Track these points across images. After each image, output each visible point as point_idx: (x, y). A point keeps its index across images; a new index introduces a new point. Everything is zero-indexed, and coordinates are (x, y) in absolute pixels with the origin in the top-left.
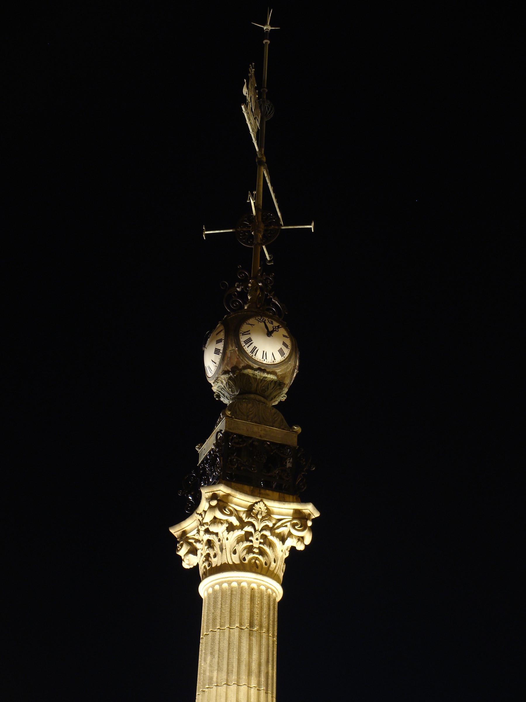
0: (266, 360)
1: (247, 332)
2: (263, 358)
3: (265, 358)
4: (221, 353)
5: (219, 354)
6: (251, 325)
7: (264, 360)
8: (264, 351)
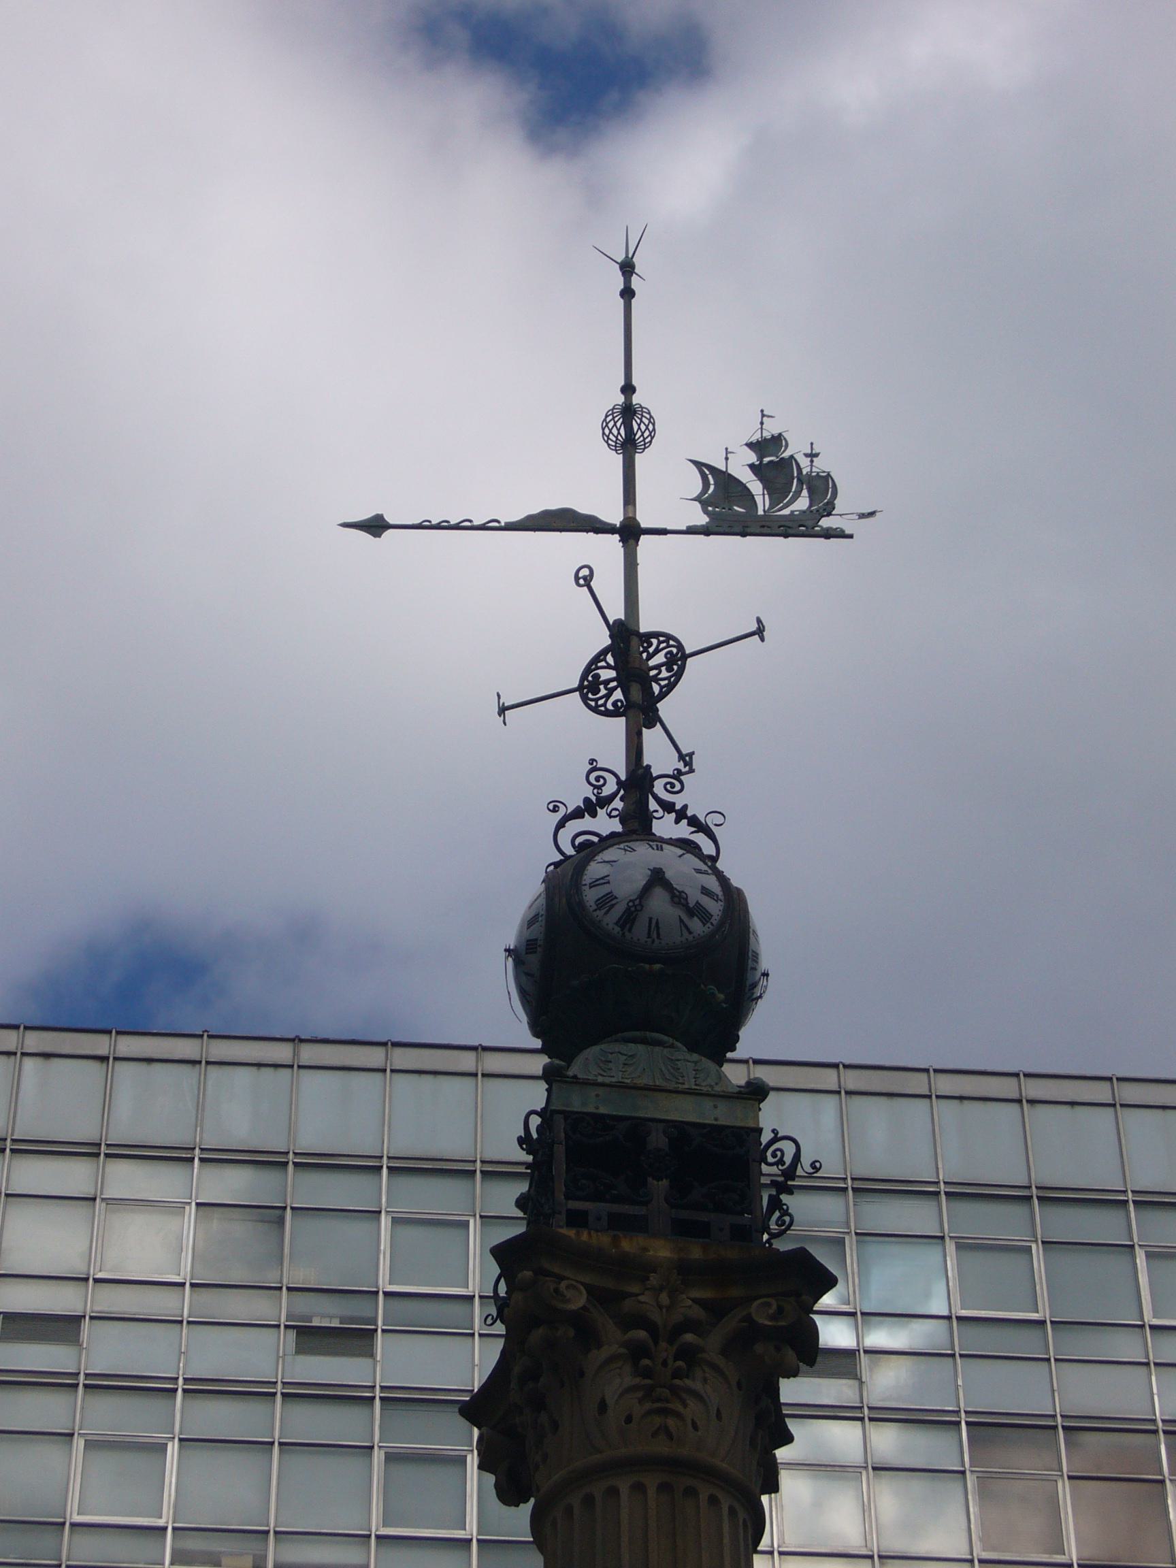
0: (657, 941)
1: (603, 878)
2: (649, 936)
3: (655, 936)
4: (540, 946)
5: (535, 952)
6: (607, 862)
7: (653, 942)
8: (650, 919)
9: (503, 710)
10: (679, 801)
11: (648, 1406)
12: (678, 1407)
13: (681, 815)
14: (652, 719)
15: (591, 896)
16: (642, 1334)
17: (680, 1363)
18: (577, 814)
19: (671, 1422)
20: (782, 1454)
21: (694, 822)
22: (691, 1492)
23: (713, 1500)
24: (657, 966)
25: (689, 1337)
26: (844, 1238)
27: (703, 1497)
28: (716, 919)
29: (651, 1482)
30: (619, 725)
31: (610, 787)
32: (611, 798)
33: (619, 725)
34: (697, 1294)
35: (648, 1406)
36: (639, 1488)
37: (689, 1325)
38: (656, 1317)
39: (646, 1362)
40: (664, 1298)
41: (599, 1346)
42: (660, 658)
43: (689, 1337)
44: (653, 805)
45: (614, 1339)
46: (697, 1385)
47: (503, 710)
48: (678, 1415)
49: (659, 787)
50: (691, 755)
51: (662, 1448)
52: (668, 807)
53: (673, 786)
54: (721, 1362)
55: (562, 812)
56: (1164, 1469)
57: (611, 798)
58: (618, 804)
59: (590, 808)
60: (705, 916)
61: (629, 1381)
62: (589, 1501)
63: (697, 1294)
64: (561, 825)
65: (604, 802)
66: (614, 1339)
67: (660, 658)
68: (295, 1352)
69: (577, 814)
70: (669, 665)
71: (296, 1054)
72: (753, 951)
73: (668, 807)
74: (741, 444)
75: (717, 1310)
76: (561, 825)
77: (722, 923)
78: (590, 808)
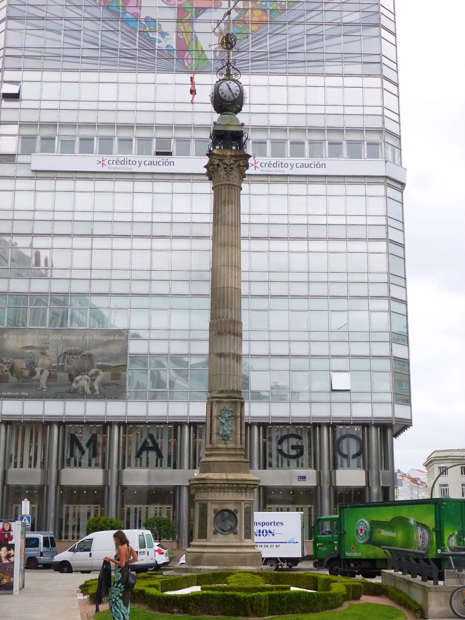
9: (210, 46)
11: (227, 176)
12: (230, 176)
15: (220, 92)
19: (229, 179)
22: (232, 188)
23: (235, 189)
24: (230, 103)
27: (233, 189)
28: (238, 95)
29: (226, 187)
35: (227, 176)
36: (225, 188)
37: (232, 164)
38: (227, 163)
39: (226, 170)
40: (229, 160)
41: (220, 167)
45: (222, 166)
46: (233, 173)
47: (210, 46)
48: (230, 177)
51: (228, 183)
54: (236, 169)
56: (21, 443)
60: (236, 94)
61: (224, 172)
62: (219, 189)
65: (224, 67)
66: (222, 166)
68: (250, 538)
69: (220, 70)
71: (191, 217)
75: (236, 161)
77: (239, 96)
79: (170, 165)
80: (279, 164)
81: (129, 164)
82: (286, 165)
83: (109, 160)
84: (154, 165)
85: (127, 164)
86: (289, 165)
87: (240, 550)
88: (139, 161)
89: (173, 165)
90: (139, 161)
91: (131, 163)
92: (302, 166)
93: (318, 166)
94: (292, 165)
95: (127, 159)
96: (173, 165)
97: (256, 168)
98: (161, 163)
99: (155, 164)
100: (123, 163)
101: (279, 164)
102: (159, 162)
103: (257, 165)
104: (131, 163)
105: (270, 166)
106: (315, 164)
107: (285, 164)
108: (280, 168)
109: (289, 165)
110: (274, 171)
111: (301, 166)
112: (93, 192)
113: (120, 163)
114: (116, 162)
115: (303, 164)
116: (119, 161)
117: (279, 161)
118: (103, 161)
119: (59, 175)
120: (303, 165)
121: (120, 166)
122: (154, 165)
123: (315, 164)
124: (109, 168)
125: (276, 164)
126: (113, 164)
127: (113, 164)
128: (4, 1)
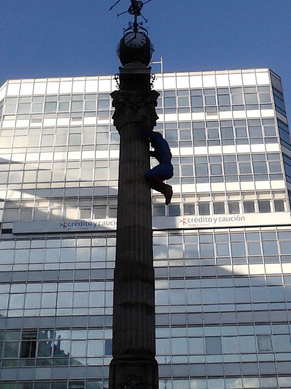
10: (142, 26)
13: (142, 28)
14: (139, 14)
16: (131, 104)
17: (137, 108)
18: (127, 30)
20: (156, 108)
21: (144, 29)
25: (138, 104)
26: (80, 218)
30: (134, 16)
31: (132, 25)
32: (132, 27)
33: (134, 16)
34: (139, 98)
37: (138, 102)
42: (139, 5)
43: (138, 104)
44: (138, 27)
49: (139, 25)
50: (80, 179)
52: (140, 27)
53: (117, 86)
55: (125, 30)
57: (132, 27)
58: (133, 28)
59: (129, 29)
63: (139, 98)
64: (125, 31)
65: (131, 28)
67: (139, 5)
69: (127, 30)
70: (140, 6)
72: (151, 48)
73: (140, 27)
74: (61, 223)
76: (125, 31)
78: (129, 29)
79: (242, 220)
80: (204, 219)
81: (206, 221)
82: (210, 220)
83: (189, 219)
84: (227, 220)
85: (204, 221)
86: (213, 219)
87: (57, 366)
88: (214, 219)
89: (244, 220)
90: (214, 219)
91: (207, 220)
92: (224, 220)
93: (238, 219)
94: (215, 219)
95: (204, 217)
96: (244, 220)
97: (184, 223)
98: (233, 219)
99: (228, 220)
100: (200, 220)
101: (204, 219)
102: (111, 223)
103: (66, 225)
104: (207, 220)
105: (196, 221)
106: (235, 218)
107: (209, 219)
108: (205, 223)
109: (213, 219)
110: (200, 225)
111: (223, 220)
112: (59, 248)
113: (198, 221)
114: (75, 224)
115: (105, 222)
116: (197, 219)
117: (204, 217)
118: (184, 220)
119: (94, 234)
120: (225, 219)
121: (198, 223)
122: (227, 220)
123: (235, 218)
124: (189, 225)
125: (202, 219)
126: (192, 222)
127: (192, 222)
128: (120, 1)
